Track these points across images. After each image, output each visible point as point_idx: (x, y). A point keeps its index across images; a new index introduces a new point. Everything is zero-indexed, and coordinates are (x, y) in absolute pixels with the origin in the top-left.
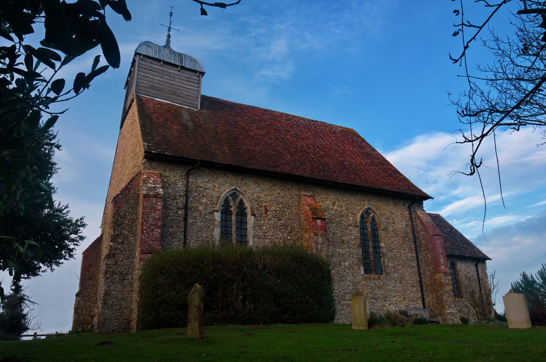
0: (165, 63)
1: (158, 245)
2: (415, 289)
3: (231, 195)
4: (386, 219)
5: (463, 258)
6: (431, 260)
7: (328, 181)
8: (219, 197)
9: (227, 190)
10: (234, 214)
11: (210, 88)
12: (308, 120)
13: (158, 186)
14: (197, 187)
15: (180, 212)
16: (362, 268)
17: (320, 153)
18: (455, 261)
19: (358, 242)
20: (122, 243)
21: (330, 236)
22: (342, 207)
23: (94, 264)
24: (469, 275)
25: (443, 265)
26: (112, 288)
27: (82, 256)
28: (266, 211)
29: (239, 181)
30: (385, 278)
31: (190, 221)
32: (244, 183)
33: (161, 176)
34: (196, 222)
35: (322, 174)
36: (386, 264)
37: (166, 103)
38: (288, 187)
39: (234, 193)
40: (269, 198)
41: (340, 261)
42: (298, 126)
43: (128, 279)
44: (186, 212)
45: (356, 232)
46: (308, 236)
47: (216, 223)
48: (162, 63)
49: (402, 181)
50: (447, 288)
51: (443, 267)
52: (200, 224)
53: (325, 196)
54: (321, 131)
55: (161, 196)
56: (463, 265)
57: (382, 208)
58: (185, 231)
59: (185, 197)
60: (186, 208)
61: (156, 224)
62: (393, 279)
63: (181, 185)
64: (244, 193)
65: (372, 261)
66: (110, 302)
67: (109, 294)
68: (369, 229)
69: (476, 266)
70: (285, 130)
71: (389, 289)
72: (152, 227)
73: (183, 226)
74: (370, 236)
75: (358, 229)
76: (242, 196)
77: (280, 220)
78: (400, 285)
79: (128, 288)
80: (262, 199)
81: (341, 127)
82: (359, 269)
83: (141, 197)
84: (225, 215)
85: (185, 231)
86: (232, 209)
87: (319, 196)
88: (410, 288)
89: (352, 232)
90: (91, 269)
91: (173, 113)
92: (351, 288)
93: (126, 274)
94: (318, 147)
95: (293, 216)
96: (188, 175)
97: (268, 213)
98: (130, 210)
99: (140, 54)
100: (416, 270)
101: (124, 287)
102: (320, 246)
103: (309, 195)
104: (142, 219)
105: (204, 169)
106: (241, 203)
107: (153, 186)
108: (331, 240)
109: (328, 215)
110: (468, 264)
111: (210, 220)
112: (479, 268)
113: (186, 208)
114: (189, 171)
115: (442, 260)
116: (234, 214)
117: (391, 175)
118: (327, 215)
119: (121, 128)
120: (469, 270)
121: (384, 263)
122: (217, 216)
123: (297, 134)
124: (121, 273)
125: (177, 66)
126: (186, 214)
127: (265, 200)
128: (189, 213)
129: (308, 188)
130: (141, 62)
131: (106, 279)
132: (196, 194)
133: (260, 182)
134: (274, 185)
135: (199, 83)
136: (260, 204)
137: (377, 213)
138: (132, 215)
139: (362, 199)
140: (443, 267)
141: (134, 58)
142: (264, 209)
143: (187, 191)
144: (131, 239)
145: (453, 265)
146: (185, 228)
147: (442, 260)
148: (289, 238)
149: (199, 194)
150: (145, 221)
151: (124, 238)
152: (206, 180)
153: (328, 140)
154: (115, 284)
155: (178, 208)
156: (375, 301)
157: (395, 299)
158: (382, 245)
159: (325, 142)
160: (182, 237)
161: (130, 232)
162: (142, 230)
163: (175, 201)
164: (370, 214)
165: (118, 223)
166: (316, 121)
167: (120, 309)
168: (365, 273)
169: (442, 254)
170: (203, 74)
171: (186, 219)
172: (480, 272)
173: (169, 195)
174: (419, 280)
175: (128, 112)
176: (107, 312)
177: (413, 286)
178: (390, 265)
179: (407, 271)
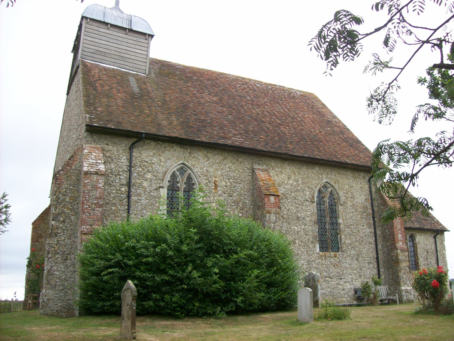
0: (112, 25)
1: (99, 225)
2: (372, 265)
3: (178, 170)
4: (344, 193)
5: (422, 230)
6: (389, 236)
7: (284, 154)
8: (165, 173)
9: (175, 165)
10: (181, 190)
11: (158, 51)
12: (266, 84)
13: (100, 161)
14: (141, 162)
15: (123, 189)
16: (318, 246)
17: (276, 122)
18: (414, 233)
19: (315, 218)
20: (64, 221)
21: (285, 212)
22: (298, 181)
23: (43, 235)
24: (427, 248)
25: (401, 241)
26: (55, 268)
27: (31, 226)
28: (216, 186)
29: (188, 155)
30: (341, 256)
31: (134, 198)
32: (192, 156)
33: (103, 150)
34: (140, 200)
35: (277, 145)
36: (343, 241)
37: (113, 69)
38: (240, 160)
39: (182, 168)
40: (219, 173)
41: (295, 239)
42: (254, 91)
43: (71, 260)
44: (129, 188)
45: (313, 208)
46: (260, 213)
47: (162, 200)
48: (109, 26)
49: (362, 152)
50: (404, 264)
51: (401, 243)
52: (144, 202)
53: (280, 170)
54: (279, 96)
55: (103, 173)
56: (422, 237)
57: (340, 181)
58: (128, 209)
59: (128, 173)
60: (129, 184)
61: (98, 203)
62: (349, 256)
63: (124, 160)
64: (192, 167)
65: (329, 239)
66: (53, 282)
67: (52, 275)
68: (327, 205)
69: (435, 237)
70: (239, 96)
71: (346, 267)
72: (93, 206)
73: (127, 204)
74: (328, 211)
75: (315, 204)
76: (190, 171)
77: (231, 196)
78: (356, 262)
79: (71, 268)
80: (212, 174)
81: (301, 91)
82: (315, 247)
83: (83, 174)
84: (171, 192)
85: (128, 209)
86: (179, 185)
87: (273, 169)
88: (366, 265)
89: (309, 208)
90: (40, 240)
91: (121, 78)
92: (305, 266)
93: (68, 254)
94: (275, 115)
95: (244, 192)
96: (131, 148)
97: (218, 189)
98: (71, 187)
99: (87, 18)
100: (374, 246)
101: (67, 267)
102: (272, 225)
103: (262, 169)
104: (83, 198)
105: (149, 142)
106: (189, 178)
107: (95, 161)
108: (285, 216)
109: (283, 189)
110: (426, 236)
111: (155, 197)
112: (437, 240)
113: (129, 184)
114: (133, 144)
115: (400, 236)
116: (181, 190)
117: (351, 145)
118: (281, 191)
119: (68, 94)
120: (427, 242)
121: (341, 239)
122: (164, 192)
123: (252, 100)
124: (63, 253)
125: (125, 29)
126: (129, 191)
127: (215, 176)
128: (133, 190)
129: (261, 161)
130: (88, 26)
131: (49, 258)
132: (140, 169)
133: (209, 155)
134: (225, 158)
135: (148, 47)
136: (210, 179)
137: (336, 187)
138: (73, 193)
139: (320, 172)
140: (401, 243)
141: (81, 22)
142: (214, 185)
143: (130, 166)
144: (72, 217)
145: (412, 238)
146: (129, 206)
147: (400, 236)
148: (240, 215)
149: (143, 169)
150: (85, 200)
151: (66, 217)
152: (151, 154)
153: (286, 107)
154: (58, 265)
155: (121, 185)
156: (330, 279)
157: (350, 276)
158: (340, 221)
159: (282, 108)
160: (125, 215)
161: (71, 210)
162: (82, 210)
163: (118, 177)
164: (328, 188)
165: (59, 201)
166: (274, 85)
167: (63, 289)
168: (320, 251)
169: (400, 230)
170: (152, 36)
171: (129, 197)
172: (438, 244)
173: (112, 170)
174: (375, 256)
175: (74, 77)
176: (51, 292)
177: (369, 263)
178: (347, 242)
179: (364, 248)
